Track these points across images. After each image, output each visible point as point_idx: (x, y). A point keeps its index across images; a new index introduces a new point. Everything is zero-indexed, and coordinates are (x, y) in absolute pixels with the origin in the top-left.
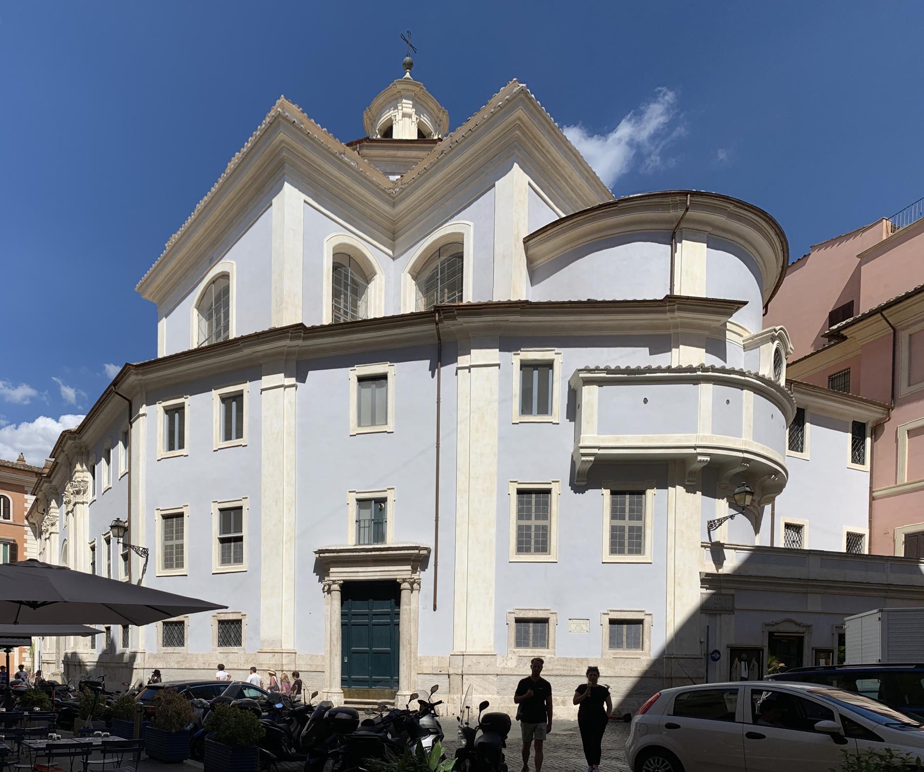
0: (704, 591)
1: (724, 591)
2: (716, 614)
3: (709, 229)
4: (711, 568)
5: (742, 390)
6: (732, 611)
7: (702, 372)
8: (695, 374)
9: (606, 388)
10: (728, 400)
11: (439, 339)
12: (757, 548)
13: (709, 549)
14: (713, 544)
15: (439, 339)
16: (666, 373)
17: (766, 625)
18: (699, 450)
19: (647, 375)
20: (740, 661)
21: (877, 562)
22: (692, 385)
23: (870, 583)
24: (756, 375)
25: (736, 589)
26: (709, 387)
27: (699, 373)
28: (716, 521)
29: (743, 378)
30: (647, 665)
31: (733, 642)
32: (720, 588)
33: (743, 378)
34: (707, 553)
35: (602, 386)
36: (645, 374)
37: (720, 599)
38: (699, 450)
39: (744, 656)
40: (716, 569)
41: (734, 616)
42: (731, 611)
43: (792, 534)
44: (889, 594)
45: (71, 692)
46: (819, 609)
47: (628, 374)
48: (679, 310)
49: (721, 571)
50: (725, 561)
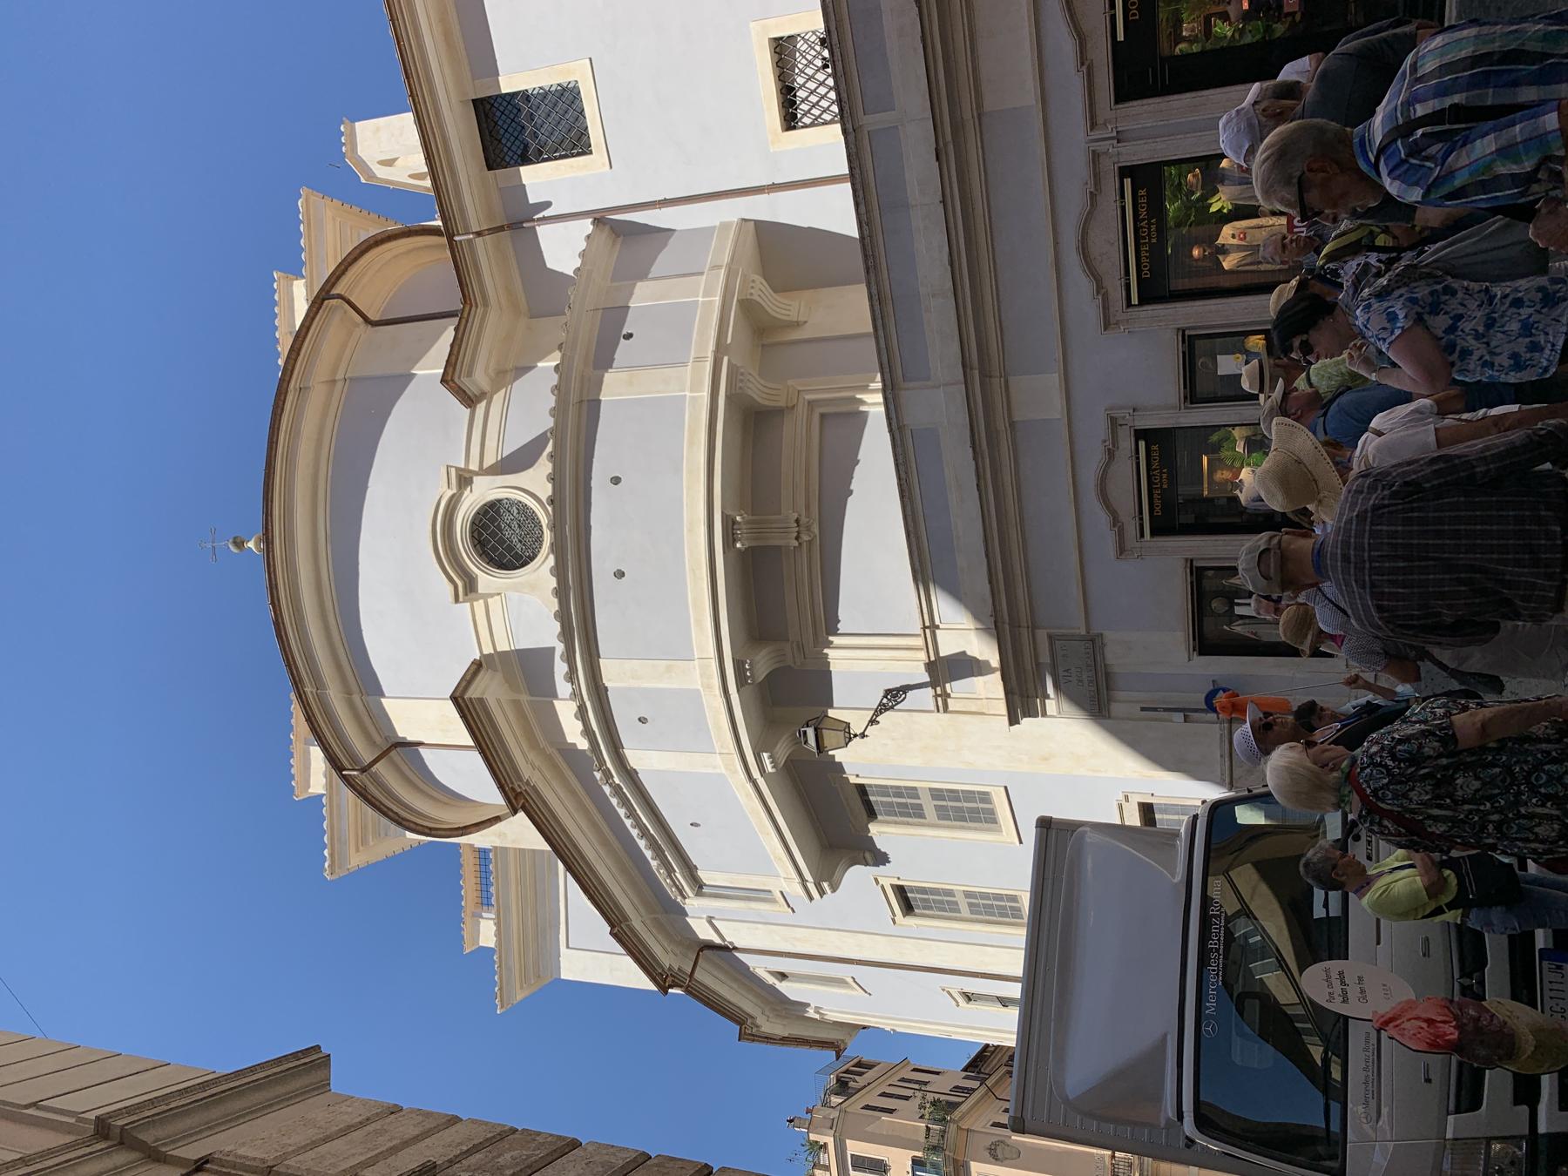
0: (1051, 705)
1: (1045, 658)
2: (1107, 675)
3: (356, 698)
4: (990, 688)
5: (606, 689)
6: (1093, 641)
7: (612, 777)
8: (621, 784)
9: (695, 859)
10: (640, 719)
11: (501, 229)
12: (919, 576)
13: (948, 685)
14: (933, 683)
15: (501, 229)
16: (638, 814)
17: (1122, 550)
18: (756, 774)
19: (652, 832)
20: (1232, 617)
21: (869, 165)
22: (639, 775)
23: (922, 32)
24: (571, 678)
25: (1034, 627)
26: (605, 665)
27: (617, 780)
28: (885, 701)
29: (588, 704)
30: (1251, 810)
31: (1177, 638)
32: (1038, 664)
33: (588, 704)
34: (956, 688)
35: (695, 866)
36: (652, 835)
37: (1067, 671)
38: (756, 774)
39: (1217, 605)
40: (993, 673)
41: (1106, 633)
42: (1094, 642)
43: (810, 78)
44: (967, 115)
45: (1394, 747)
46: (1054, 379)
47: (663, 852)
48: (520, 778)
49: (995, 662)
50: (969, 653)
